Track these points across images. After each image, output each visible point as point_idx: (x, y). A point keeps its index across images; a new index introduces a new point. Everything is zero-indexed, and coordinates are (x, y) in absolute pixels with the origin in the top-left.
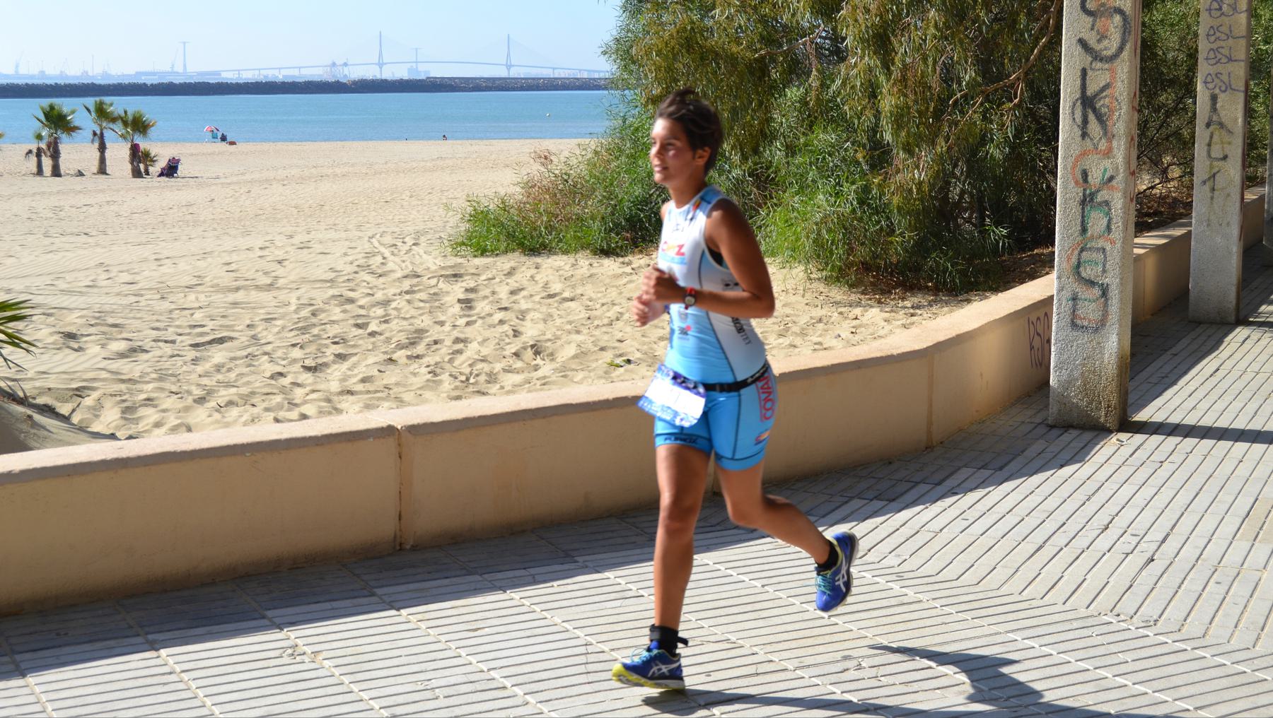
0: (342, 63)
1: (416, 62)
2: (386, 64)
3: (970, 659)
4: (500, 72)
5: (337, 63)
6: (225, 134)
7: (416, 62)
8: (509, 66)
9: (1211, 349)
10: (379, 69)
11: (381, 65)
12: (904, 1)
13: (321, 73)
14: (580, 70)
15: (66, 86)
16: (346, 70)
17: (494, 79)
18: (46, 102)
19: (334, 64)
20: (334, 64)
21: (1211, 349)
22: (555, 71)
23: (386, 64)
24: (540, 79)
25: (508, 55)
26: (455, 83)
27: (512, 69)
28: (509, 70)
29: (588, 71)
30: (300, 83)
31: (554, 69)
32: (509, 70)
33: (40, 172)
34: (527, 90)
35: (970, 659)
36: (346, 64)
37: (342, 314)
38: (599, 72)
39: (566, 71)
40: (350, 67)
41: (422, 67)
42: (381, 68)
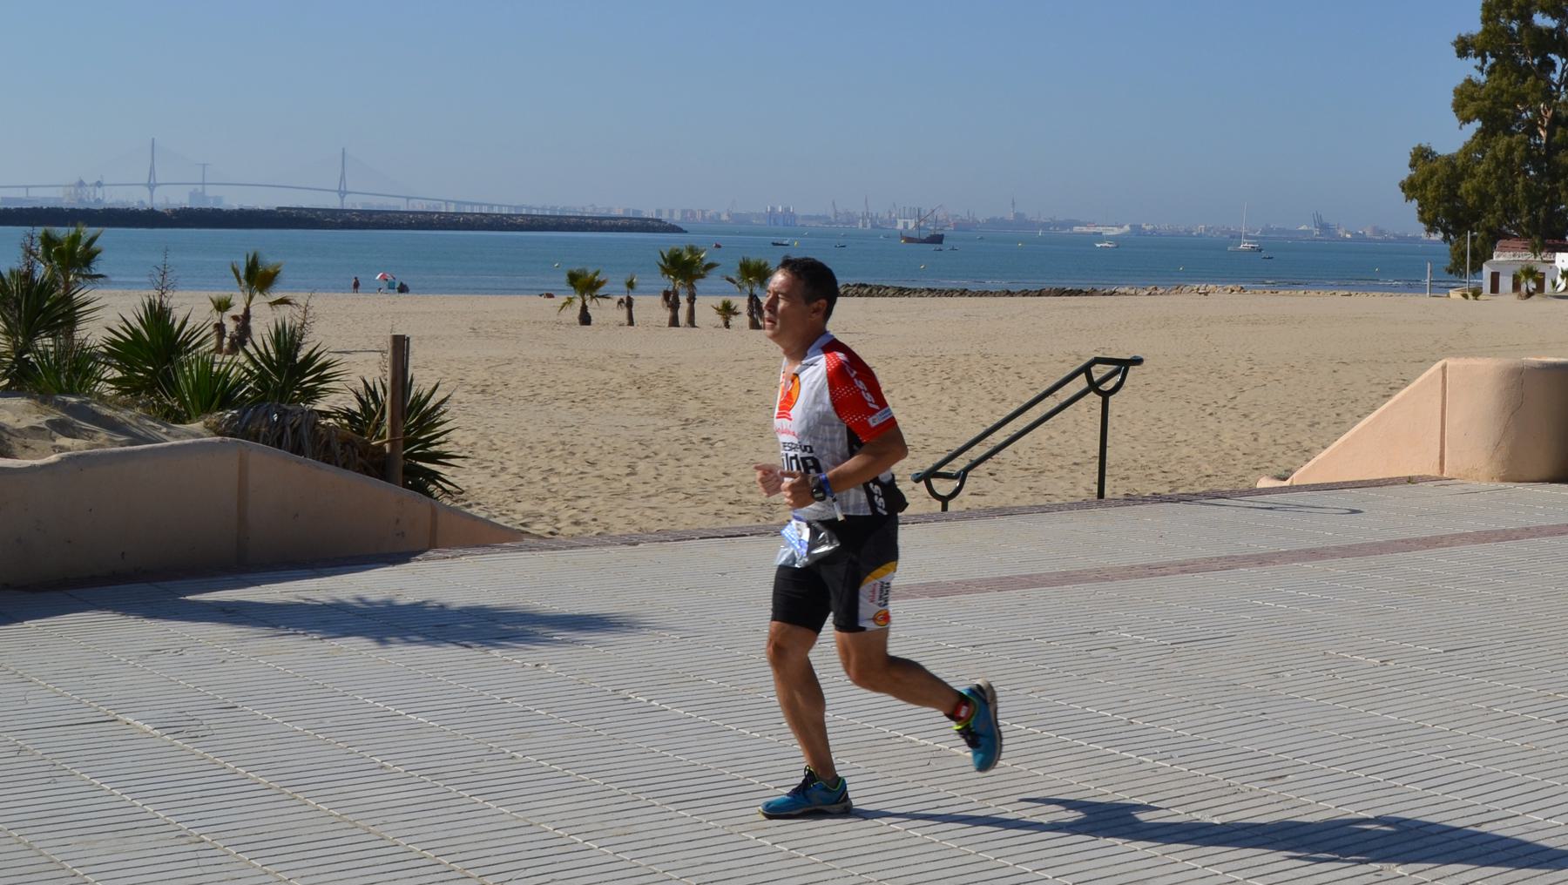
0: (94, 182)
1: (203, 184)
2: (350, 193)
3: (1432, 857)
4: (332, 202)
5: (87, 182)
6: (404, 283)
7: (203, 184)
8: (343, 193)
9: (1158, 828)
10: (149, 192)
11: (151, 186)
12: (1539, 2)
13: (61, 195)
14: (447, 202)
15: (20, 211)
16: (99, 193)
17: (371, 213)
18: (39, 231)
19: (81, 184)
20: (81, 184)
21: (1158, 828)
22: (411, 202)
23: (350, 193)
24: (434, 213)
25: (342, 177)
26: (318, 216)
27: (347, 196)
28: (342, 198)
29: (499, 205)
30: (97, 211)
31: (408, 198)
32: (342, 198)
33: (674, 322)
34: (418, 229)
35: (1432, 857)
36: (99, 184)
37: (575, 451)
38: (472, 204)
39: (428, 202)
40: (106, 188)
41: (211, 192)
42: (152, 191)
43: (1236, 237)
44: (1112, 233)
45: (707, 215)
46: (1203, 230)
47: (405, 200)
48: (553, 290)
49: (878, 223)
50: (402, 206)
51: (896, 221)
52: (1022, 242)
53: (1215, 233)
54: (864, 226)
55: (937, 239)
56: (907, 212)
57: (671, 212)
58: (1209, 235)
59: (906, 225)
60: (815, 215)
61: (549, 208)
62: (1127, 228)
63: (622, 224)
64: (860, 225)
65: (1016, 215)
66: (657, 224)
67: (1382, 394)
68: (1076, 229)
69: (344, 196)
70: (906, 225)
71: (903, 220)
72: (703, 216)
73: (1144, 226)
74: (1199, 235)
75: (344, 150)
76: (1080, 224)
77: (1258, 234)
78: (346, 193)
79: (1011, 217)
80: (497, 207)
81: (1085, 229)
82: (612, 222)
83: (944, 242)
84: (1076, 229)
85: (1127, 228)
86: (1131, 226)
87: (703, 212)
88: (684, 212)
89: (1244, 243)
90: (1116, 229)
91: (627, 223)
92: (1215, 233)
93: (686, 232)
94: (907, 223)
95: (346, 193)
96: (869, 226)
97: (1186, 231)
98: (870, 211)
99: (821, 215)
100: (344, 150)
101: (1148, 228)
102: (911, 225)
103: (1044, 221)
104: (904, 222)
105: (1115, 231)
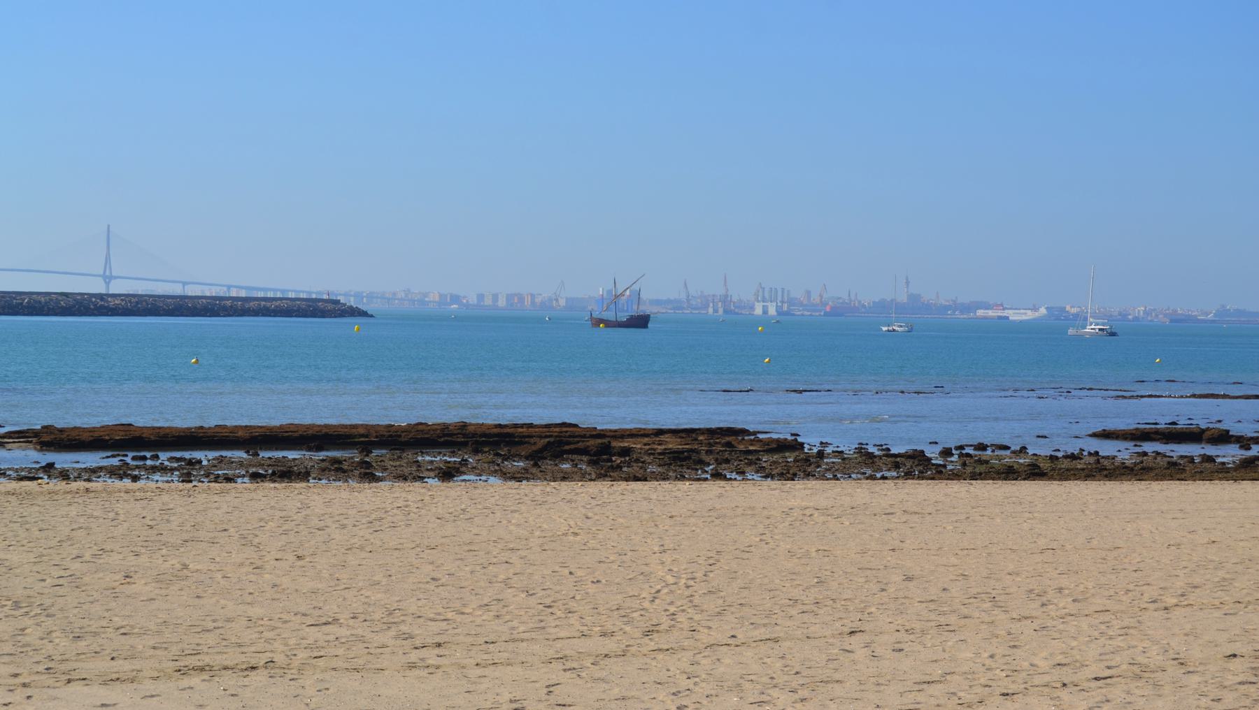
2: (116, 278)
4: (93, 286)
8: (108, 279)
11: (108, 279)
23: (116, 278)
28: (108, 284)
32: (108, 284)
43: (1081, 319)
44: (1024, 318)
45: (538, 300)
46: (1142, 312)
47: (181, 285)
48: (1071, 389)
49: (732, 308)
50: (176, 290)
51: (754, 305)
52: (95, 298)
53: (1157, 316)
54: (716, 311)
55: (640, 322)
56: (767, 295)
57: (495, 297)
58: (1149, 318)
59: (765, 312)
60: (664, 298)
61: (352, 293)
62: (1043, 311)
63: (264, 306)
64: (711, 310)
65: (912, 297)
66: (330, 306)
67: (119, 598)
68: (980, 313)
69: (109, 282)
70: (765, 312)
71: (762, 304)
72: (533, 303)
73: (1068, 308)
74: (1136, 319)
75: (109, 226)
76: (987, 307)
77: (1210, 316)
78: (112, 278)
79: (902, 298)
80: (235, 290)
81: (991, 313)
82: (263, 303)
83: (649, 325)
84: (980, 313)
85: (1043, 311)
86: (1047, 308)
87: (533, 296)
88: (510, 297)
89: (1091, 325)
90: (1029, 312)
91: (284, 304)
92: (1157, 316)
93: (372, 316)
94: (767, 306)
95: (112, 278)
96: (721, 311)
97: (1120, 314)
98: (729, 293)
99: (672, 298)
100: (109, 226)
101: (1074, 310)
102: (772, 311)
103: (944, 303)
104: (763, 306)
105: (1029, 315)
